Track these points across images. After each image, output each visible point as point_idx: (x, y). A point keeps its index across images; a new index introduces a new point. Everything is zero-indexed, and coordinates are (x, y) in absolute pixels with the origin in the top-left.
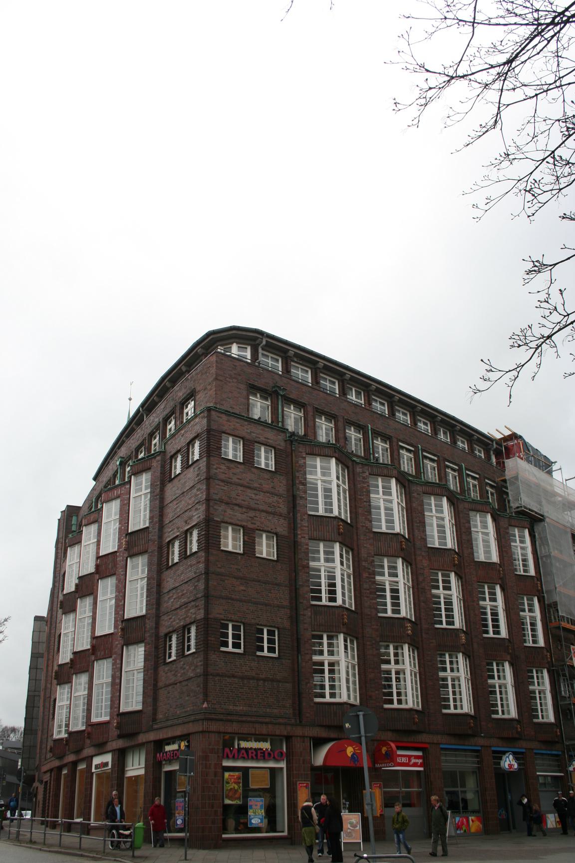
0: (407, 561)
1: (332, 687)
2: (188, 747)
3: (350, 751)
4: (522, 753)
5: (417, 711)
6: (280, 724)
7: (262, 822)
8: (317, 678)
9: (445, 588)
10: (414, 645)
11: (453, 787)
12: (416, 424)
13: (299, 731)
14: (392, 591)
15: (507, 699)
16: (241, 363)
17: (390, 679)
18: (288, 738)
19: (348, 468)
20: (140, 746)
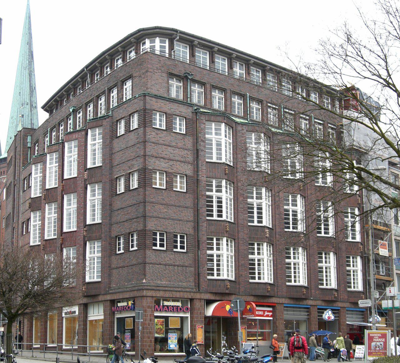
1: (218, 270)
2: (134, 304)
3: (228, 308)
4: (338, 310)
5: (270, 284)
6: (187, 292)
7: (176, 346)
8: (209, 265)
9: (293, 205)
11: (364, 321)
13: (198, 296)
14: (258, 209)
16: (164, 58)
17: (254, 264)
18: (192, 300)
20: (99, 302)
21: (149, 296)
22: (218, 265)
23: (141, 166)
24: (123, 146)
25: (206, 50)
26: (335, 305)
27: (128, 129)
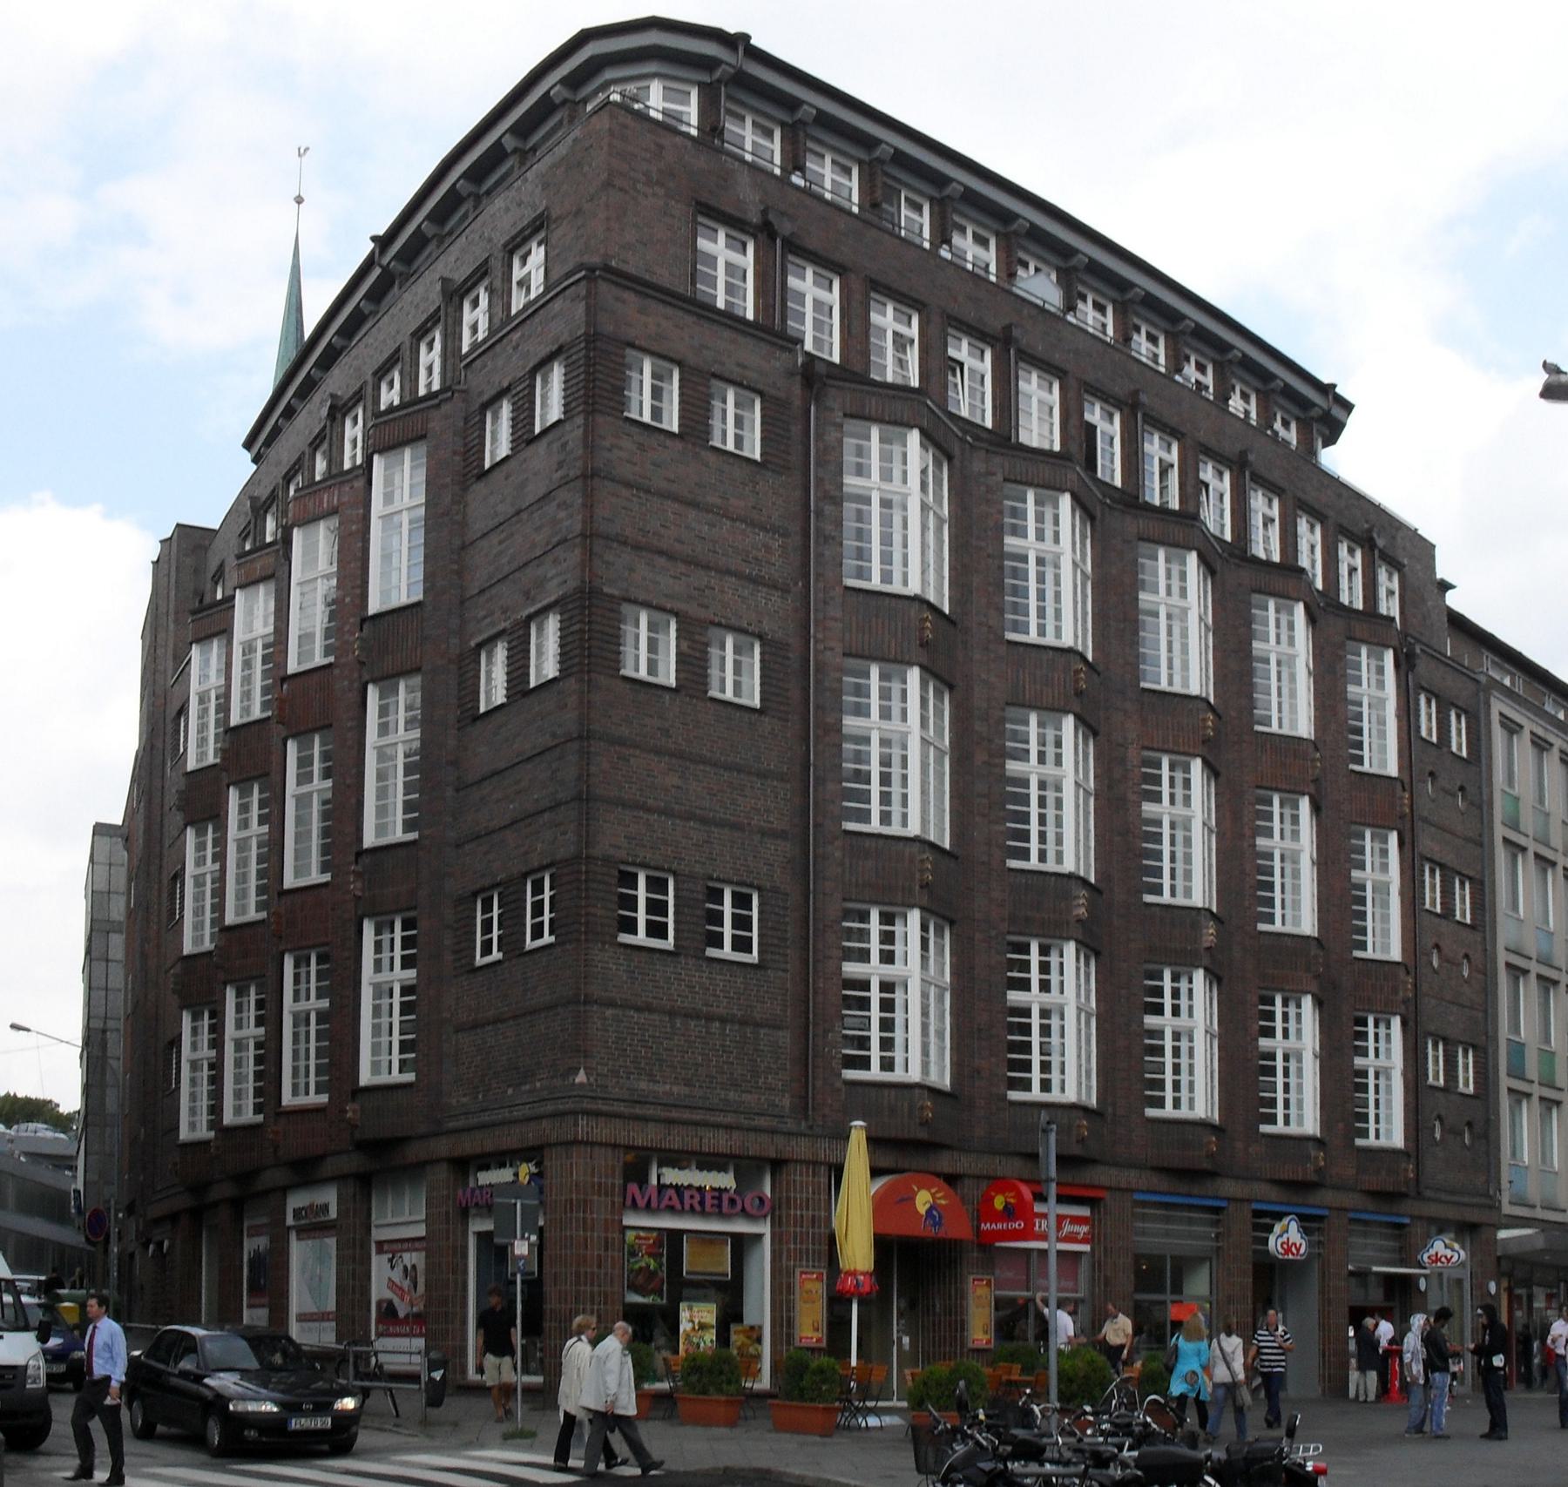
0: (1088, 726)
1: (887, 1044)
3: (923, 1200)
4: (1320, 1218)
6: (756, 1130)
10: (1090, 947)
11: (1402, 1263)
12: (1127, 340)
15: (1300, 1087)
16: (678, 139)
17: (1026, 1029)
18: (777, 1165)
19: (950, 458)
21: (601, 1144)
22: (887, 1025)
23: (573, 584)
24: (506, 509)
25: (851, 157)
26: (1311, 1201)
27: (524, 437)
